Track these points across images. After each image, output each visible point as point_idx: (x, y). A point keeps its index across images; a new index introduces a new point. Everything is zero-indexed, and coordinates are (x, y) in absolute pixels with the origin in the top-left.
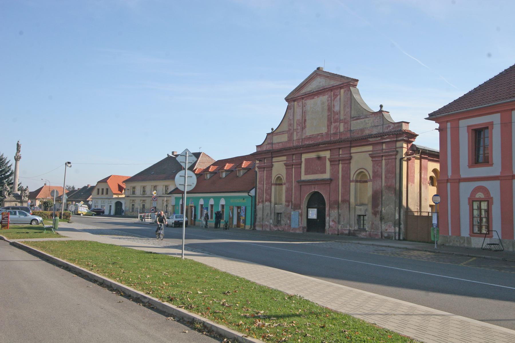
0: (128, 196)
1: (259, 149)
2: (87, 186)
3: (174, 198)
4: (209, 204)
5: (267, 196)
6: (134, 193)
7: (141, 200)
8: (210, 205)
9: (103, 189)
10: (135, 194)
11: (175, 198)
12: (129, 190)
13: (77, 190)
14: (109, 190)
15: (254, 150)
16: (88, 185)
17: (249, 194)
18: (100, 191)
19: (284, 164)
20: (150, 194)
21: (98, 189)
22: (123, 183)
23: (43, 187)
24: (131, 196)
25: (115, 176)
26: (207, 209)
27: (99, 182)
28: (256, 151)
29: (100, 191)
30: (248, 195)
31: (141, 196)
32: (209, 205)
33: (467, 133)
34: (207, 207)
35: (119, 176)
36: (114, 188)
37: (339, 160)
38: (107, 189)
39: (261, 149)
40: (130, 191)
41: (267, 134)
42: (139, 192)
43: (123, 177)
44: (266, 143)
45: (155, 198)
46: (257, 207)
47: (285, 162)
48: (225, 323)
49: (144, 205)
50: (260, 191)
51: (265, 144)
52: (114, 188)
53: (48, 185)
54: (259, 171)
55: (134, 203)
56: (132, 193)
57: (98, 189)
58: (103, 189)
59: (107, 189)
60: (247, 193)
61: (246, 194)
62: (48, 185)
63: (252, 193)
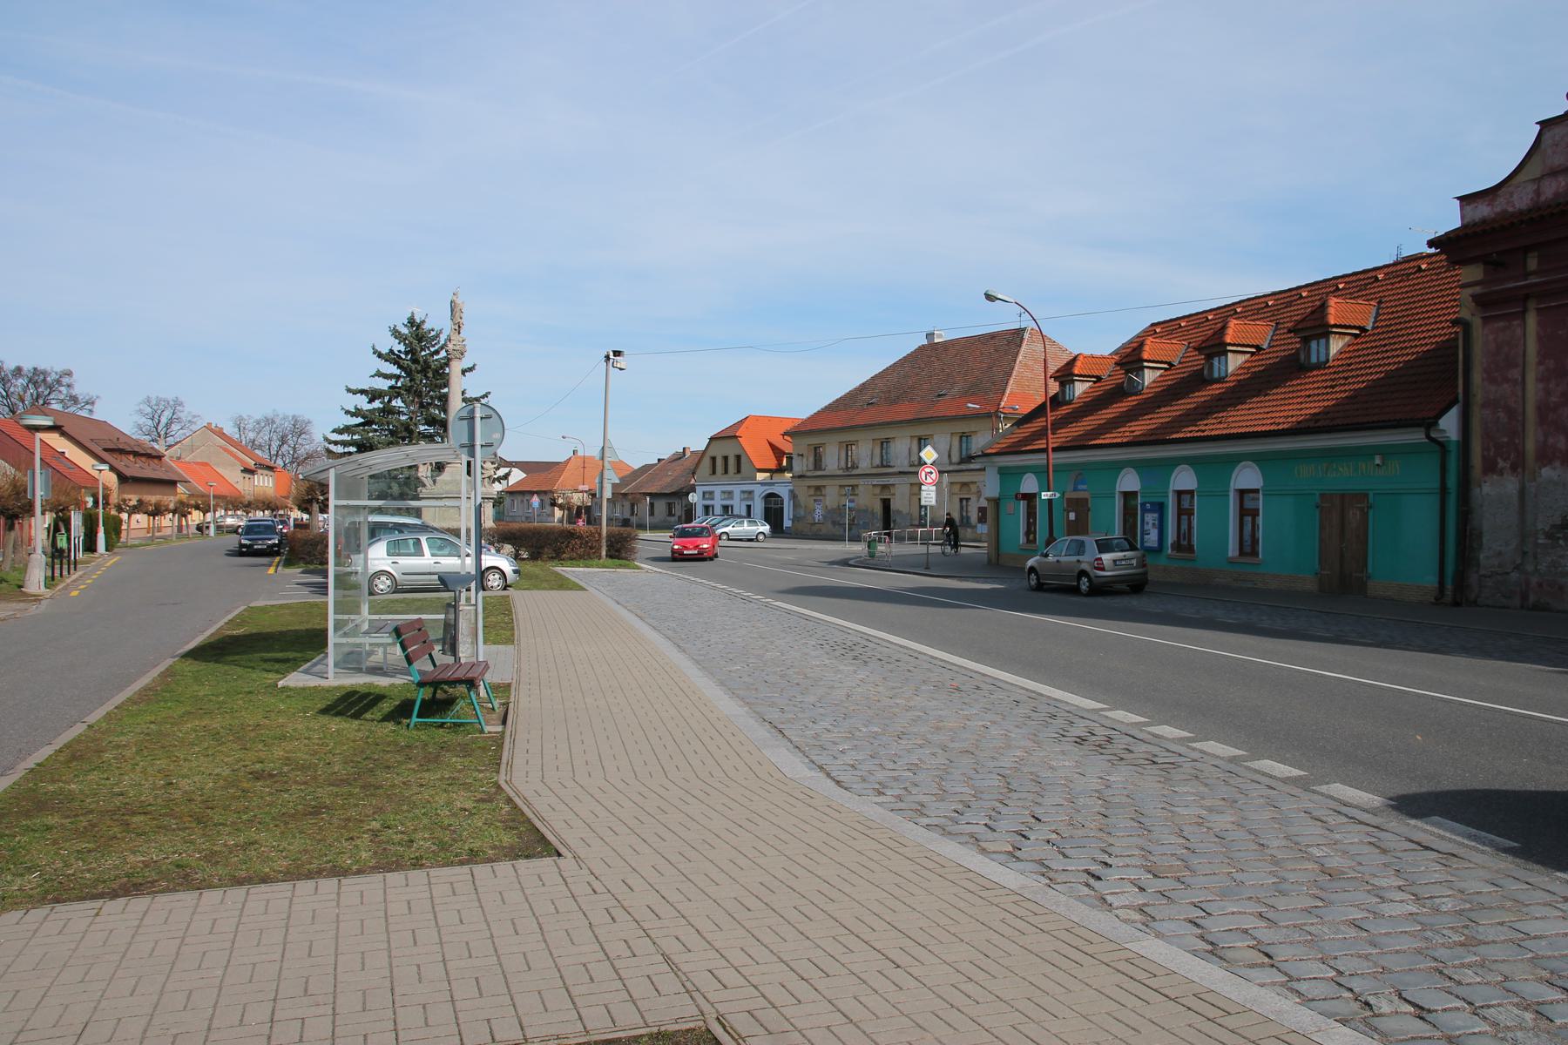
0: (801, 477)
1: (1483, 211)
2: (682, 451)
3: (996, 472)
4: (1171, 488)
5: (1551, 440)
6: (818, 464)
7: (809, 487)
8: (1122, 496)
9: (726, 458)
10: (823, 467)
11: (999, 473)
12: (802, 455)
13: (656, 465)
14: (743, 460)
15: (1450, 220)
16: (684, 449)
17: (1433, 435)
18: (719, 462)
19: (1474, 297)
20: (870, 466)
21: (714, 459)
22: (783, 435)
23: (570, 458)
24: (809, 474)
25: (757, 418)
26: (1160, 508)
27: (712, 439)
28: (1457, 224)
29: (719, 462)
30: (1428, 436)
31: (840, 472)
32: (1170, 495)
33: (1392, 262)
34: (1161, 500)
35: (770, 419)
36: (759, 455)
37: (1526, 298)
38: (738, 458)
39: (1498, 209)
40: (805, 460)
41: (1538, 127)
42: (486, 513)
43: (781, 420)
44: (1534, 170)
45: (931, 473)
46: (1476, 491)
47: (1478, 290)
48: (85, 735)
49: (889, 500)
50: (1501, 415)
51: (1521, 177)
52: (759, 455)
53: (580, 453)
54: (1486, 320)
55: (822, 495)
56: (811, 467)
57: (714, 459)
58: (726, 458)
59: (738, 458)
60: (1423, 429)
61: (1416, 436)
62: (580, 453)
63: (1449, 424)
